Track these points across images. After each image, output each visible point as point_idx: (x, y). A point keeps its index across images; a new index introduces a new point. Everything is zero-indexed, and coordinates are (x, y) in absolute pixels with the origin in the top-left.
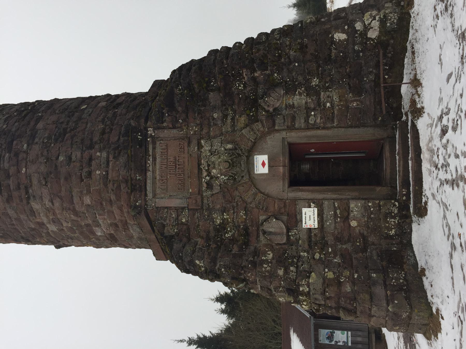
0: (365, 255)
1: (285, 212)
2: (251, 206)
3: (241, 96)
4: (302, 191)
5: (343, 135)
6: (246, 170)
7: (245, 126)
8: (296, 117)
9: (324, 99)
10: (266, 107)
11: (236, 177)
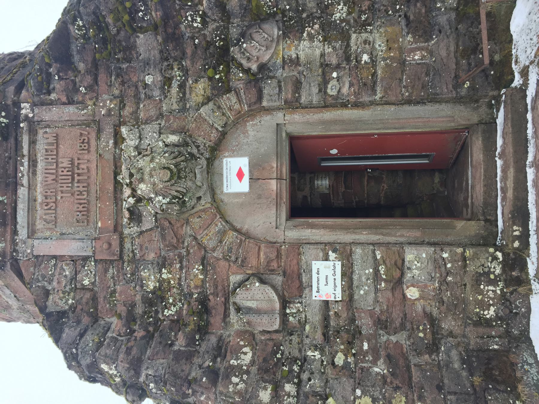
1: (279, 267)
2: (215, 255)
3: (197, 41)
5: (392, 119)
7: (206, 101)
8: (301, 83)
9: (358, 48)
10: (244, 62)
11: (187, 199)
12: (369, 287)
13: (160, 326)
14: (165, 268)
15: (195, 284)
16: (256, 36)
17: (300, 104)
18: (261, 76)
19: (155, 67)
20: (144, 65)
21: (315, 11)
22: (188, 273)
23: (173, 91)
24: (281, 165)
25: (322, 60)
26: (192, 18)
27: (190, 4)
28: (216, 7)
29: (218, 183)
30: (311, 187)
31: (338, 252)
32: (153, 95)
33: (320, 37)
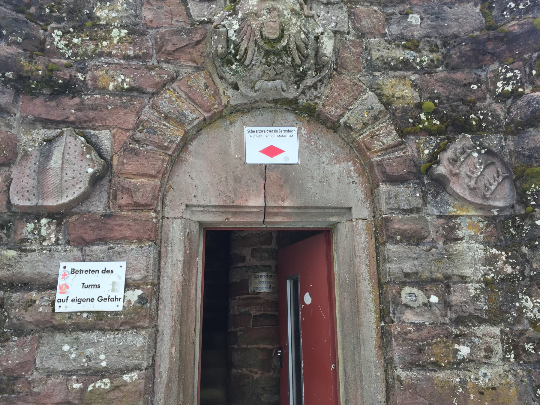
1: (120, 207)
2: (146, 109)
3: (475, 87)
4: (188, 263)
5: (362, 396)
6: (254, 94)
7: (385, 99)
8: (417, 245)
9: (479, 338)
10: (449, 154)
11: (234, 67)
12: (75, 360)
13: (36, 23)
14: (128, 34)
15: (100, 76)
16: (491, 172)
17: (384, 243)
18: (426, 182)
19: (433, 27)
20: (435, 14)
21: (535, 266)
22: (118, 67)
23: (398, 52)
24: (286, 215)
25: (455, 279)
26: (510, 78)
27: (534, 72)
28: (532, 112)
29: (260, 118)
30: (256, 267)
31: (140, 305)
32: (391, 24)
33: (493, 275)
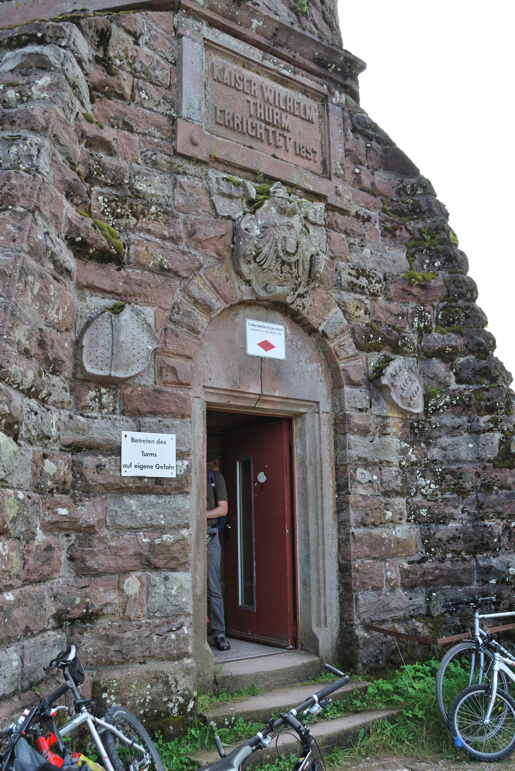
0: (50, 627)
